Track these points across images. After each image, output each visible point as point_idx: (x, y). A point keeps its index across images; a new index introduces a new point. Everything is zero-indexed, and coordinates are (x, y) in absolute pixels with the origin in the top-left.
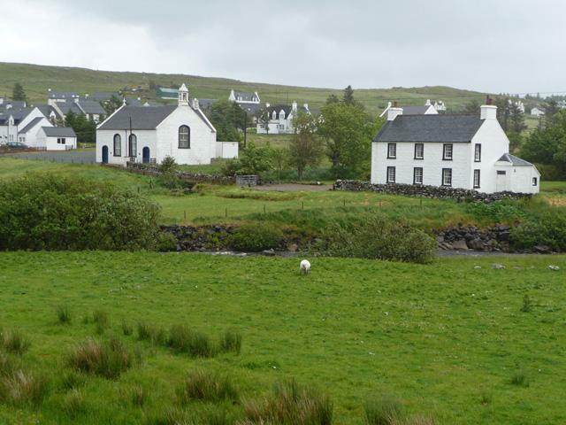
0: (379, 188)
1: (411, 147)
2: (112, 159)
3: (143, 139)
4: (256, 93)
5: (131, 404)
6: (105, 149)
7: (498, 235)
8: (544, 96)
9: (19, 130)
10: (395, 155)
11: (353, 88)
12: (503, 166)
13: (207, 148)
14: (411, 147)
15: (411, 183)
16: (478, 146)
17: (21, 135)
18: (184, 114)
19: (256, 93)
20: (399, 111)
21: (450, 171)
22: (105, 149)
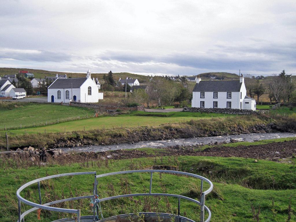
0: (194, 110)
1: (212, 94)
2: (56, 100)
3: (73, 92)
4: (66, 75)
5: (40, 187)
6: (53, 97)
7: (272, 127)
8: (181, 76)
9: (1, 90)
10: (231, 97)
11: (113, 72)
12: (247, 100)
13: (97, 97)
14: (212, 94)
15: (212, 108)
16: (241, 93)
17: (3, 92)
18: (89, 82)
19: (66, 75)
20: (200, 80)
21: (217, 102)
22: (53, 97)
